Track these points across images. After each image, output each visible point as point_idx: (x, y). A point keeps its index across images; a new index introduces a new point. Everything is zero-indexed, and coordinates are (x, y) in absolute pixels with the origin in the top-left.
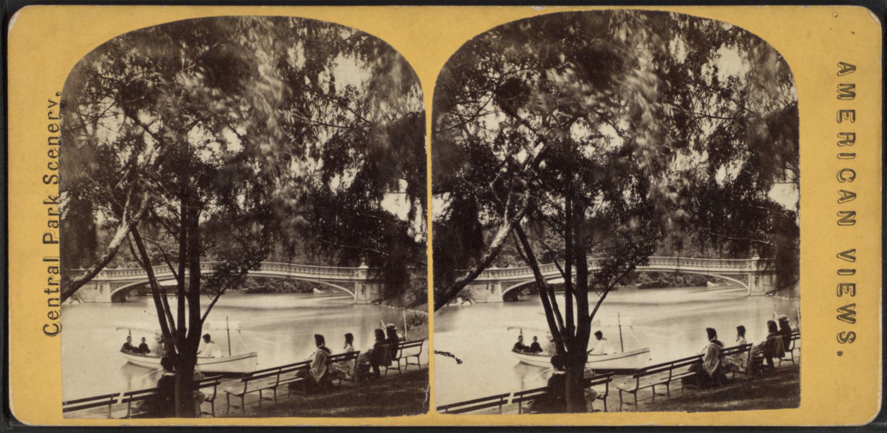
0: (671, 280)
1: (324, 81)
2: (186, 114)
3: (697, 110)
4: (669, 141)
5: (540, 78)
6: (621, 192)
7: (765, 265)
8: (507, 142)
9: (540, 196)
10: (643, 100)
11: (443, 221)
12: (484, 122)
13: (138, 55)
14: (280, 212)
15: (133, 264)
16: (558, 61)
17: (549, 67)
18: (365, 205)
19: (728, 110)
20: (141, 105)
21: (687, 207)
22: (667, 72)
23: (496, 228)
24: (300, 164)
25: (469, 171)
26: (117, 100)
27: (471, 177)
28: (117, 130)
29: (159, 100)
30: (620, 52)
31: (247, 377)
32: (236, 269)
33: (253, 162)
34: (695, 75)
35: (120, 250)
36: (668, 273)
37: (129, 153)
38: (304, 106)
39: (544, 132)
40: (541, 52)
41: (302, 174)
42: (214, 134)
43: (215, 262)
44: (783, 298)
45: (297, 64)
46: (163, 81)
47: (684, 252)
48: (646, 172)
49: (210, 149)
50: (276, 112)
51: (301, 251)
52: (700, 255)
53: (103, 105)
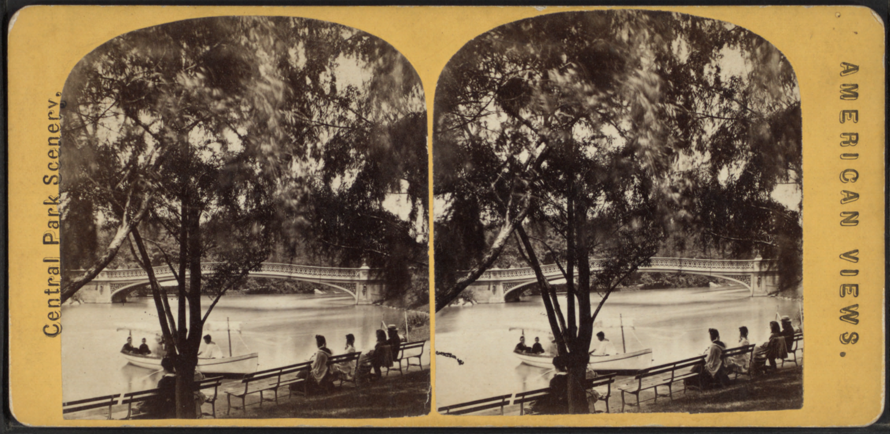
0: (673, 281)
1: (325, 82)
2: (187, 114)
3: (700, 111)
4: (671, 141)
5: (542, 78)
6: (623, 192)
7: (767, 266)
8: (508, 142)
9: (542, 197)
10: (646, 100)
11: (445, 221)
12: (485, 122)
13: (139, 55)
14: (281, 213)
15: (133, 264)
16: (560, 61)
17: (551, 68)
18: (366, 205)
19: (730, 110)
20: (141, 105)
21: (690, 208)
22: (669, 72)
23: (498, 229)
24: (301, 165)
25: (470, 172)
26: (117, 100)
27: (472, 177)
28: (118, 130)
29: (160, 100)
30: (622, 52)
31: (248, 378)
32: (237, 269)
33: (254, 162)
34: (697, 75)
35: (120, 251)
36: (671, 273)
37: (130, 153)
38: (305, 106)
39: (546, 132)
40: (543, 52)
41: (303, 175)
42: (214, 135)
43: (216, 262)
44: (786, 298)
45: (298, 64)
46: (164, 81)
47: (687, 253)
48: (648, 173)
49: (211, 150)
50: (277, 112)
51: (302, 252)
52: (703, 255)
53: (103, 105)
